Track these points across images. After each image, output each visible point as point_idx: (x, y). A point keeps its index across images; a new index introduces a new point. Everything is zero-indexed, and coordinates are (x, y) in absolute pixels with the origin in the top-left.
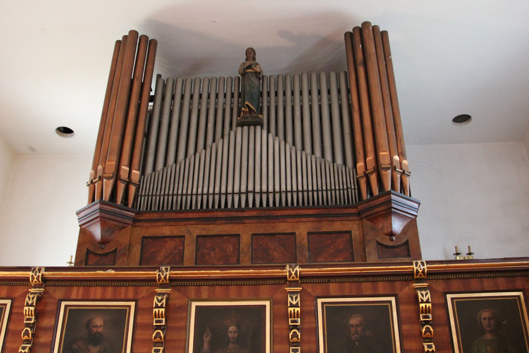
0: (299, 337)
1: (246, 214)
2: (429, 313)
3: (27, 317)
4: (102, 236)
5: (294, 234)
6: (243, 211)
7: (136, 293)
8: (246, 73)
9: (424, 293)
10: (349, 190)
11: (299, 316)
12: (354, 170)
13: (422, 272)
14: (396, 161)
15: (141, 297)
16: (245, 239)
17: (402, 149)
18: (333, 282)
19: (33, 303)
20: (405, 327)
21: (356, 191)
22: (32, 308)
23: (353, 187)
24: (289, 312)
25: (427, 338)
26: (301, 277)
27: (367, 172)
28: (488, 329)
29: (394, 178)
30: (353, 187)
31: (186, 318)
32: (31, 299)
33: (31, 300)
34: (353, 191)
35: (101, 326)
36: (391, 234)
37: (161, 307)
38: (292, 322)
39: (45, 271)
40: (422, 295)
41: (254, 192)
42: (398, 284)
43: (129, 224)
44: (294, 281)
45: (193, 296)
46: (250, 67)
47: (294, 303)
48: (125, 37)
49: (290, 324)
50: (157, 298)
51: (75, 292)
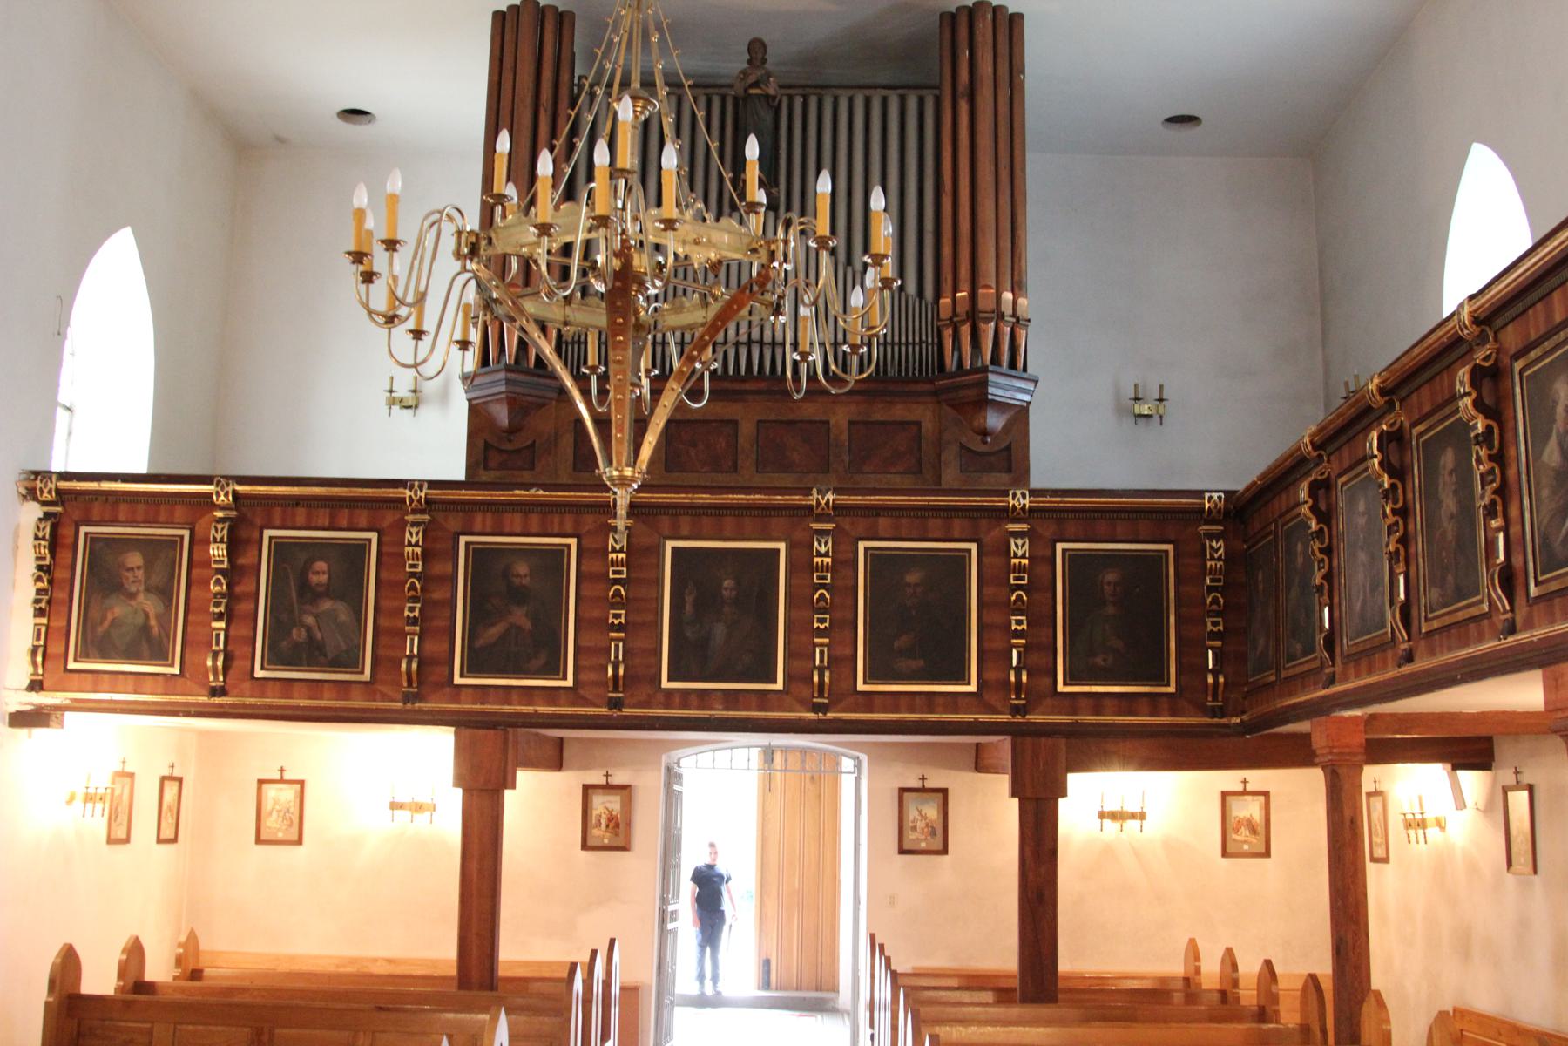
0: (829, 601)
1: (747, 386)
2: (1024, 572)
3: (411, 562)
4: (509, 423)
5: (828, 422)
6: (743, 380)
7: (577, 523)
8: (750, 95)
9: (1020, 542)
10: (924, 346)
11: (830, 570)
12: (935, 307)
13: (1021, 509)
14: (1006, 301)
15: (585, 531)
16: (747, 429)
17: (1020, 274)
18: (884, 516)
19: (418, 541)
20: (987, 591)
21: (936, 348)
22: (418, 550)
23: (930, 340)
24: (815, 564)
25: (1018, 609)
26: (835, 507)
27: (955, 319)
28: (1111, 599)
29: (1001, 333)
30: (930, 340)
31: (658, 565)
32: (413, 536)
33: (414, 536)
34: (930, 348)
35: (526, 576)
36: (984, 433)
37: (621, 551)
38: (819, 578)
39: (429, 488)
40: (1017, 546)
41: (761, 343)
42: (984, 523)
43: (551, 399)
44: (823, 514)
45: (666, 532)
46: (756, 85)
47: (823, 550)
48: (511, 8)
49: (816, 581)
50: (613, 537)
51: (479, 520)
